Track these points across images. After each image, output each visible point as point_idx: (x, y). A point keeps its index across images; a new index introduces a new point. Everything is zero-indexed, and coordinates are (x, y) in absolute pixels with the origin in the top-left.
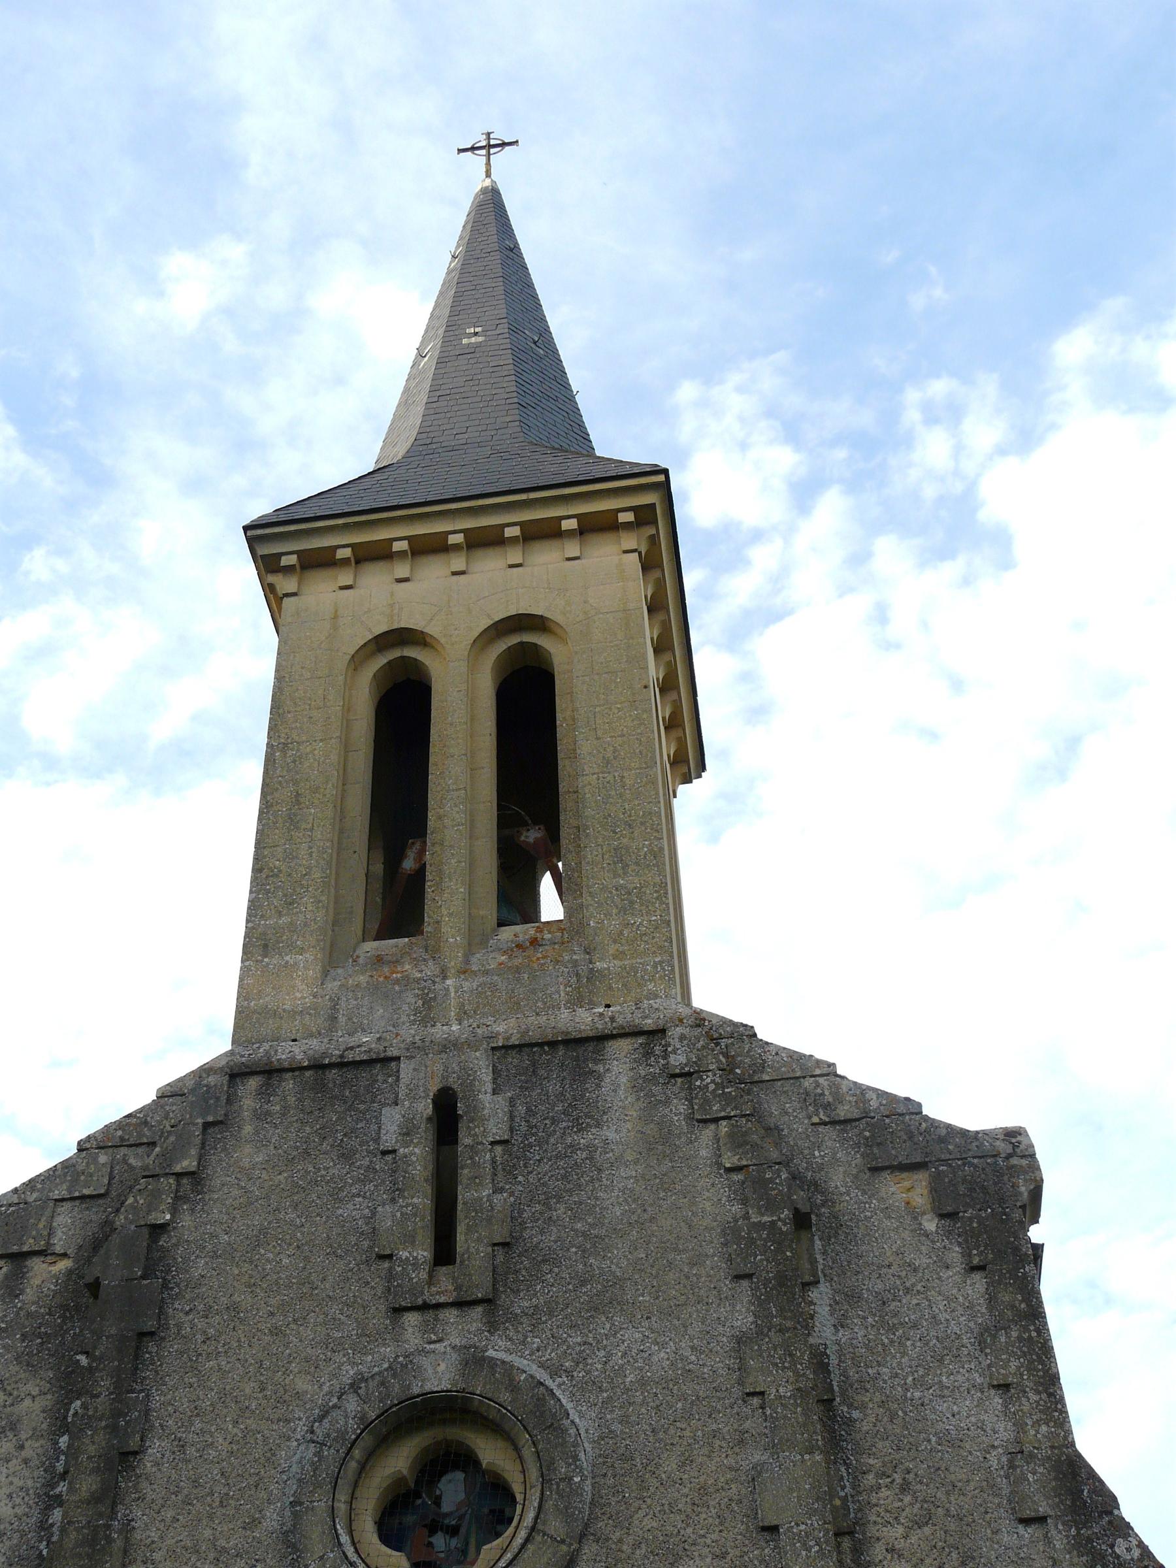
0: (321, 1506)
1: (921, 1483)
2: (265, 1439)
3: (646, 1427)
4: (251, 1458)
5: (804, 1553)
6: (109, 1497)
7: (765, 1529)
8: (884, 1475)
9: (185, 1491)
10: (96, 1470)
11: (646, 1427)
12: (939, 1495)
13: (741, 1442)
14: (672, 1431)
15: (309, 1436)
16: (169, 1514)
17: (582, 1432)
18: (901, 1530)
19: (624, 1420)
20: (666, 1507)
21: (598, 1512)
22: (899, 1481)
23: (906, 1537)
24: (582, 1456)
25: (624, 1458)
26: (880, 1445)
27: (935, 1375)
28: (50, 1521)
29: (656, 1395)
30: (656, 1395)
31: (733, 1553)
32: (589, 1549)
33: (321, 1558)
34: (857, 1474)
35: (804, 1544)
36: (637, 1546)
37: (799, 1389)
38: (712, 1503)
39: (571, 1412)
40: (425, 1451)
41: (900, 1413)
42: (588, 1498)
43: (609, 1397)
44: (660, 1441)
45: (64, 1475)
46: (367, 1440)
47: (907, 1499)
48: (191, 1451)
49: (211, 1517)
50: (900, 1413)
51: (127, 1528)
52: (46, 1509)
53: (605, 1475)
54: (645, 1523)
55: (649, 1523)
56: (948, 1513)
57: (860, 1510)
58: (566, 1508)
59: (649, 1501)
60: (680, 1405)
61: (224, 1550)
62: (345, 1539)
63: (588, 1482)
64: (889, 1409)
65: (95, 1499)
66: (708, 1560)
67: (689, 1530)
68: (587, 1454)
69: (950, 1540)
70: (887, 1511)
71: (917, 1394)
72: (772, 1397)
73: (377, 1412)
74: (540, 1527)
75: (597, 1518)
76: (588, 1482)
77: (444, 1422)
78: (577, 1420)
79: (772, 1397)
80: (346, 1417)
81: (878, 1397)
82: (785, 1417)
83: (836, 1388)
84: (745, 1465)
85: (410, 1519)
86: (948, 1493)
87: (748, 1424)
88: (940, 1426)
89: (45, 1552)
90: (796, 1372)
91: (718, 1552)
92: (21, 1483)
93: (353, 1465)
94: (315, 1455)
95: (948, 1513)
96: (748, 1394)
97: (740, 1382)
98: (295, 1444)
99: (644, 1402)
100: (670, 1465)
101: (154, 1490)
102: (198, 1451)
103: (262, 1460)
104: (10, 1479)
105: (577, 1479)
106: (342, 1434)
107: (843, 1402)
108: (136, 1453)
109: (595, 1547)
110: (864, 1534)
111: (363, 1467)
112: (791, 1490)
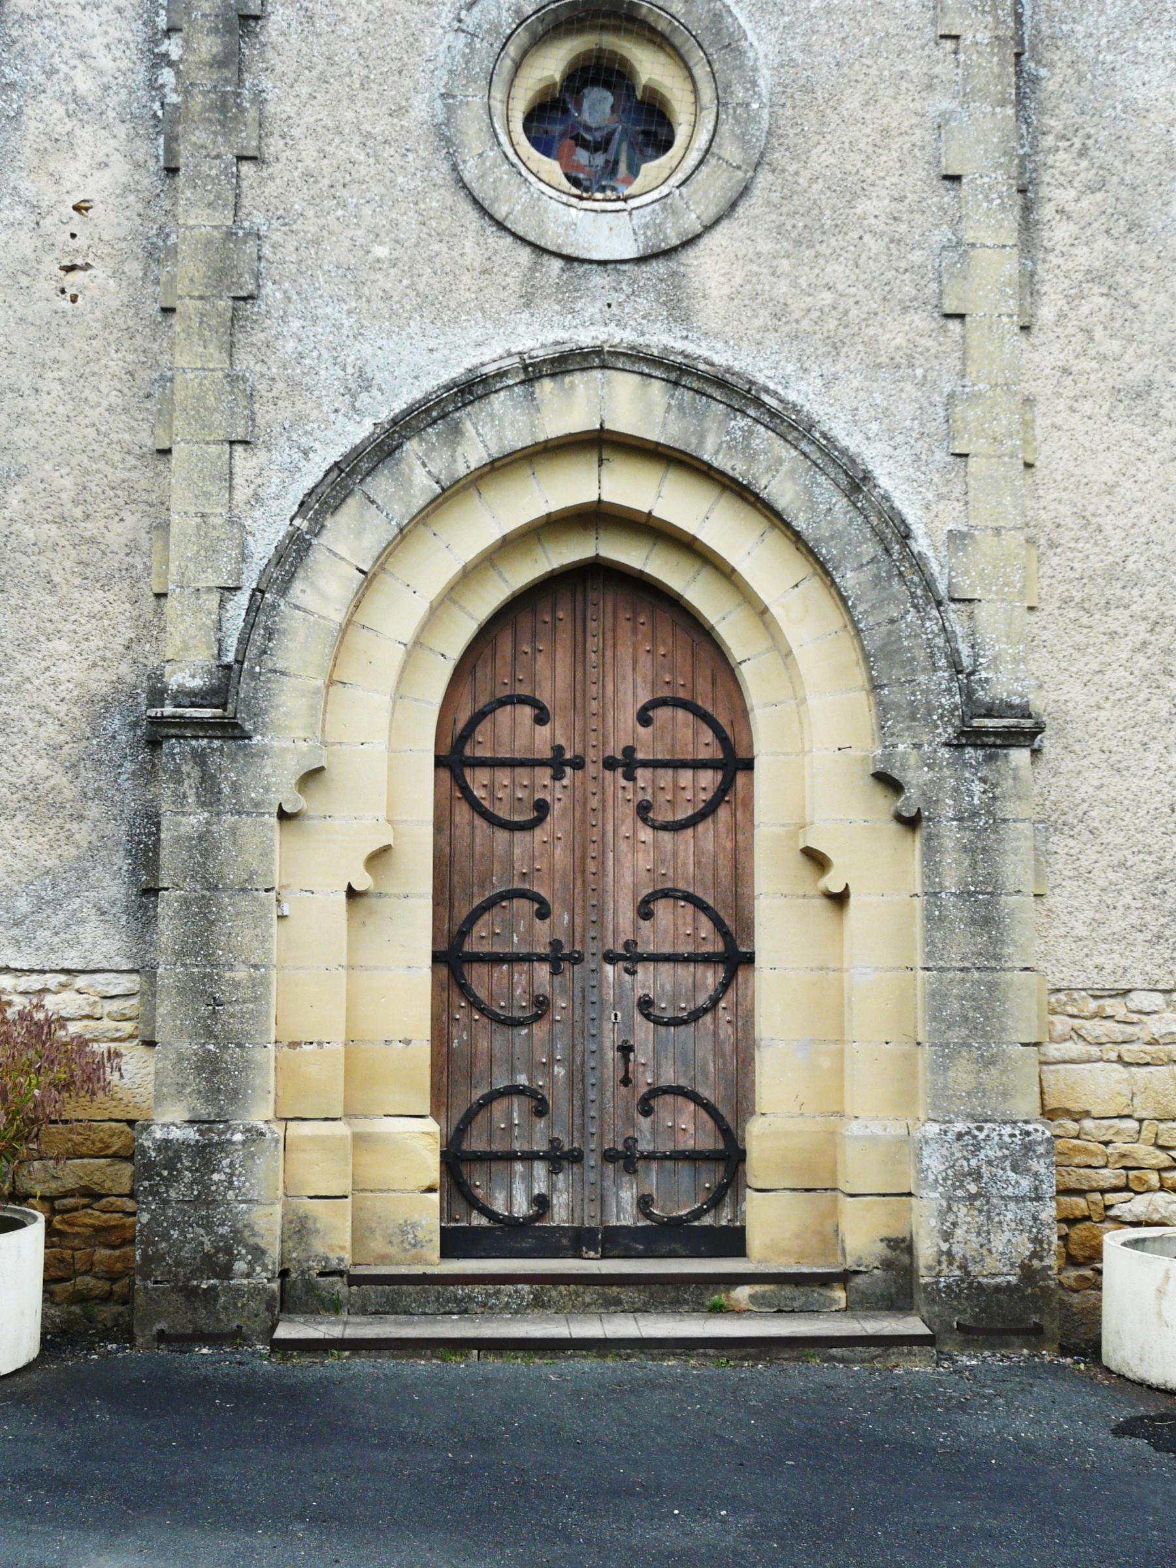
0: (477, 101)
1: (1100, 149)
2: (406, 22)
3: (829, 59)
4: (391, 41)
5: (985, 205)
6: (231, 62)
7: (946, 177)
8: (1063, 137)
9: (320, 68)
10: (215, 30)
11: (829, 59)
12: (1116, 163)
13: (930, 87)
14: (857, 67)
15: (456, 25)
16: (304, 90)
17: (761, 56)
18: (1073, 193)
19: (806, 49)
20: (846, 146)
21: (774, 141)
22: (1078, 145)
23: (1077, 200)
24: (761, 82)
25: (804, 89)
26: (1064, 107)
27: (1131, 39)
28: (160, 81)
29: (842, 26)
30: (842, 26)
31: (911, 197)
32: (764, 179)
33: (480, 155)
34: (1039, 133)
35: (986, 196)
36: (814, 180)
37: (997, 38)
38: (894, 146)
39: (749, 34)
40: (586, 55)
41: (1089, 76)
42: (765, 125)
43: (791, 22)
44: (844, 76)
45: (169, 32)
46: (522, 38)
47: (1084, 164)
48: (321, 25)
49: (352, 99)
50: (1089, 76)
51: (259, 99)
52: (153, 66)
53: (783, 105)
54: (822, 158)
55: (827, 159)
56: (1122, 181)
57: (1035, 170)
58: (744, 134)
59: (829, 137)
60: (867, 40)
61: (369, 136)
62: (503, 139)
63: (766, 110)
64: (1078, 71)
65: (219, 63)
66: (886, 202)
67: (869, 171)
68: (765, 79)
69: (1120, 208)
70: (1062, 174)
71: (1109, 58)
72: (968, 42)
73: (534, 7)
74: (714, 149)
75: (773, 148)
76: (766, 110)
77: (603, 28)
78: (756, 43)
79: (968, 42)
80: (499, 8)
81: (1068, 57)
82: (980, 65)
83: (1027, 42)
84: (932, 112)
85: (558, 129)
86: (1125, 162)
87: (937, 70)
88: (1128, 93)
89: (160, 113)
90: (996, 18)
91: (897, 196)
92: (118, 35)
93: (508, 63)
94: (466, 45)
95: (1122, 181)
96: (942, 37)
97: (934, 22)
98: (440, 31)
99: (829, 33)
100: (852, 102)
101: (283, 62)
102: (329, 25)
103: (404, 45)
104: (105, 27)
105: (755, 106)
106: (495, 27)
107: (1032, 58)
108: (257, 18)
109: (770, 177)
110: (1036, 193)
111: (518, 66)
112: (978, 141)
